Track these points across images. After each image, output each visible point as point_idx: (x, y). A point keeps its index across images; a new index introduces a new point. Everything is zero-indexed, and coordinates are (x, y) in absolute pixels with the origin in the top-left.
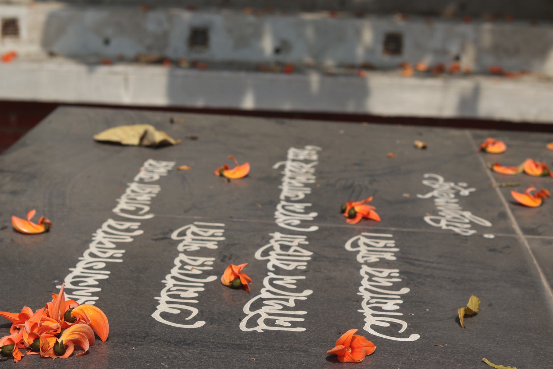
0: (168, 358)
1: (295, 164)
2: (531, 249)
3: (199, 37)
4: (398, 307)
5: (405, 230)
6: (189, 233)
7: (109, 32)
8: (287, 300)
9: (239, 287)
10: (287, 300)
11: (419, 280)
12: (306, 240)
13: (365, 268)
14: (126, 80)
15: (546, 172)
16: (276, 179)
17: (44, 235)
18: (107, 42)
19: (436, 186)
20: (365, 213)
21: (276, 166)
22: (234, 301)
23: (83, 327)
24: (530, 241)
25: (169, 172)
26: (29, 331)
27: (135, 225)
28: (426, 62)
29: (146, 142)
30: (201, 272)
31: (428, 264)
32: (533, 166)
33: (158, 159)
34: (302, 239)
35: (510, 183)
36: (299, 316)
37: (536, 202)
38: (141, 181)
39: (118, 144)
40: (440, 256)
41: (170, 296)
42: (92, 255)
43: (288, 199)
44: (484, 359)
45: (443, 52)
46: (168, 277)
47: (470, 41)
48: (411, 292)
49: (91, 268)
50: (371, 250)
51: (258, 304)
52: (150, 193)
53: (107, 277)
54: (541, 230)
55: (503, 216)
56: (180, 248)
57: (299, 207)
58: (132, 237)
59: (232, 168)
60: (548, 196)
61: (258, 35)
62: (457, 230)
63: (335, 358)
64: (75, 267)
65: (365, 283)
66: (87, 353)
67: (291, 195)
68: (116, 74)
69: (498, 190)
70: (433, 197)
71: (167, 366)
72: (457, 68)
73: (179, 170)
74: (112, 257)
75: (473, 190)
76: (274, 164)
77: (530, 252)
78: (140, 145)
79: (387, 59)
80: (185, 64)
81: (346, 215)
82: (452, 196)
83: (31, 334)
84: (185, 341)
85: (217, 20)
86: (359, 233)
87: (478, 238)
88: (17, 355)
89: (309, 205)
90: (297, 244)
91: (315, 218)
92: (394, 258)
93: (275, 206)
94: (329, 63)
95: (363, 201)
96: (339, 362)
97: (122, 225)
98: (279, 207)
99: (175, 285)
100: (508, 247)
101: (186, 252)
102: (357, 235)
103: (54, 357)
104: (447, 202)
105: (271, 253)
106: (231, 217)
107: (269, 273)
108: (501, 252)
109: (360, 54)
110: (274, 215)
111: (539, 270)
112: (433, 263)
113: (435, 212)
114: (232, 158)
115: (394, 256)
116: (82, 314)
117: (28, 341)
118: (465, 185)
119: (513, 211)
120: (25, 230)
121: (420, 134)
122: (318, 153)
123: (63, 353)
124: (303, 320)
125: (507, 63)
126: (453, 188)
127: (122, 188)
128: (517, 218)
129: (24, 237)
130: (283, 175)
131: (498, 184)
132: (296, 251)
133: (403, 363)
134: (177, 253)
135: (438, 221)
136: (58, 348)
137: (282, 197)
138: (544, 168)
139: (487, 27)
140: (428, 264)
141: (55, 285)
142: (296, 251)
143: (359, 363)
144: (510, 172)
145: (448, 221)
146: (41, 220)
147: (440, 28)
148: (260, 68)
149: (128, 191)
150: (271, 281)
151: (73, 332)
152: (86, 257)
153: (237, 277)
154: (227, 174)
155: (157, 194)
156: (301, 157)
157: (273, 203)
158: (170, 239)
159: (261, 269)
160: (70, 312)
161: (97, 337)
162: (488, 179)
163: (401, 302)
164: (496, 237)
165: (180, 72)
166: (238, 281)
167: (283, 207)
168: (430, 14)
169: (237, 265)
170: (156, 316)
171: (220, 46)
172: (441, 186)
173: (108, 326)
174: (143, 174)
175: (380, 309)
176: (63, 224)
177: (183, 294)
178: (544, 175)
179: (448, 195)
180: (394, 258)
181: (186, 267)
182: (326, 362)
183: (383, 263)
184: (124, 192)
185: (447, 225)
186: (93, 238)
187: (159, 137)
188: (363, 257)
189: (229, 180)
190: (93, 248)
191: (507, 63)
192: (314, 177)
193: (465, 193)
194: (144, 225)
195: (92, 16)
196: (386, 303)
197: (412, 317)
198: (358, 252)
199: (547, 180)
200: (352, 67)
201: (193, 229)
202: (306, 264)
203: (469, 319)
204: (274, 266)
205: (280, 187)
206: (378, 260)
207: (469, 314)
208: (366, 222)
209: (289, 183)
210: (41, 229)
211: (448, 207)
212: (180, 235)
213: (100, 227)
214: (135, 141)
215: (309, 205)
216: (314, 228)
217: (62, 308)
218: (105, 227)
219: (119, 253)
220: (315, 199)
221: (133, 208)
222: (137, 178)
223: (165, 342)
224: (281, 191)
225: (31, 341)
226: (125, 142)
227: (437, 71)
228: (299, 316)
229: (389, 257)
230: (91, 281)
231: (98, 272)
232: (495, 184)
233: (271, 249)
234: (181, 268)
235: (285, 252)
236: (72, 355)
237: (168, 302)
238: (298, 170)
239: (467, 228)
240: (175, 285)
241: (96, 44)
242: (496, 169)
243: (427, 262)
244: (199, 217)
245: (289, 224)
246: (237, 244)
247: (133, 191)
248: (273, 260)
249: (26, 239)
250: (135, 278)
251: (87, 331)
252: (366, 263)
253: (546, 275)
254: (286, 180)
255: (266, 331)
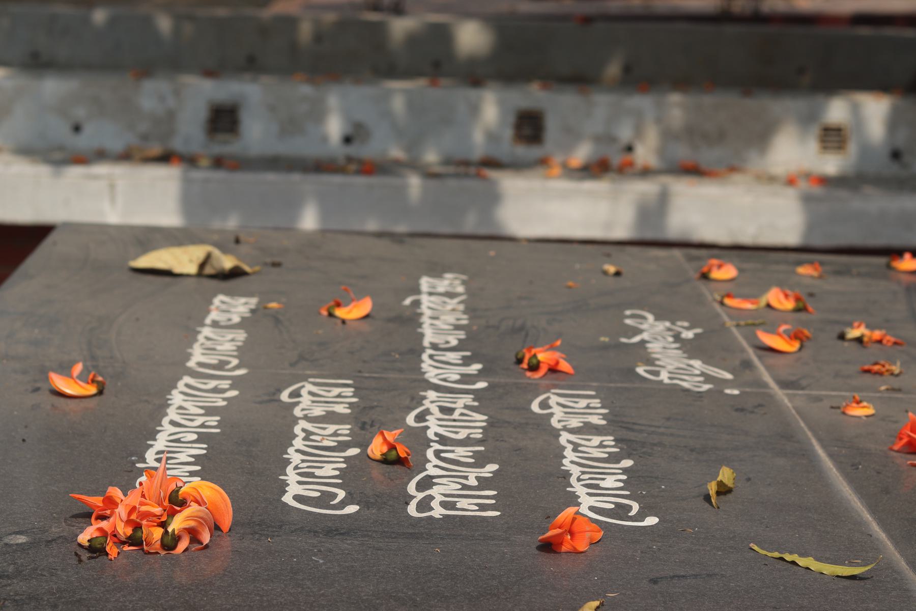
0: (320, 551)
1: (433, 298)
2: (794, 408)
3: (223, 119)
4: (621, 484)
5: (612, 385)
6: (304, 392)
7: (80, 113)
8: (466, 478)
9: (393, 461)
10: (466, 478)
11: (644, 450)
12: (474, 400)
13: (564, 437)
14: (112, 187)
15: (801, 305)
16: (412, 319)
17: (97, 398)
18: (77, 129)
19: (644, 326)
20: (552, 363)
21: (408, 301)
22: (392, 480)
23: (199, 511)
24: (791, 398)
25: (253, 311)
26: (124, 516)
27: (225, 384)
28: (582, 154)
29: (208, 270)
30: (336, 444)
31: (653, 429)
32: (782, 297)
33: (231, 293)
34: (468, 400)
35: (750, 321)
36: (488, 497)
37: (792, 345)
38: (215, 324)
39: (167, 273)
40: (668, 419)
41: (300, 474)
42: (173, 423)
43: (434, 346)
44: (752, 545)
45: (607, 139)
46: (291, 450)
47: (650, 123)
48: (635, 465)
49: (178, 441)
50: (570, 413)
51: (427, 483)
52: (233, 340)
53: (205, 452)
54: (804, 383)
55: (747, 365)
56: (297, 412)
57: (453, 357)
58: (224, 399)
59: (346, 305)
60: (808, 338)
61: (318, 114)
62: (685, 385)
63: (549, 547)
64: (155, 440)
65: (569, 454)
66: (207, 546)
67: (438, 340)
68: (96, 177)
69: (734, 330)
70: (643, 342)
71: (321, 561)
72: (631, 164)
73: (266, 308)
74: (203, 426)
75: (699, 331)
76: (404, 299)
77: (794, 412)
78: (200, 274)
79: (523, 151)
80: (204, 162)
81: (525, 366)
82: (671, 339)
83: (129, 522)
84: (337, 530)
85: (251, 92)
86: (547, 390)
87: (717, 393)
88: (112, 550)
89: (468, 354)
90: (462, 406)
91: (480, 371)
92: (604, 422)
93: (420, 356)
94: (431, 157)
95: (547, 347)
96: (555, 552)
97: (205, 384)
98: (425, 357)
99: (303, 461)
100: (760, 405)
101: (306, 418)
102: (545, 393)
103: (163, 553)
104: (664, 348)
105: (428, 417)
106: (360, 372)
107: (432, 444)
108: (752, 412)
109: (478, 143)
110: (421, 368)
111: (809, 434)
112: (659, 427)
113: (649, 361)
114: (346, 290)
115: (603, 419)
116: (195, 494)
117: (124, 531)
118: (686, 324)
119: (760, 358)
120: (69, 391)
121: (608, 255)
122: (464, 283)
123: (174, 547)
124: (493, 502)
125: (707, 156)
126: (669, 329)
127: (191, 336)
128: (768, 368)
129: (69, 401)
130: (421, 314)
131: (734, 323)
132: (462, 414)
133: (642, 552)
134: (295, 420)
135: (657, 373)
136: (168, 540)
137: (426, 343)
138: (798, 299)
139: (675, 98)
140: (653, 429)
141: (134, 463)
142: (462, 414)
143: (582, 552)
144: (748, 306)
145: (670, 373)
146: (91, 377)
147: (602, 102)
148: (321, 166)
149: (201, 338)
150: (437, 454)
151: (188, 518)
152: (167, 428)
153: (392, 447)
154: (340, 313)
155: (244, 342)
156: (441, 289)
157: (417, 351)
158: (280, 401)
159: (419, 438)
160: (178, 491)
161: (217, 528)
162: (718, 315)
163: (624, 477)
164: (742, 393)
165: (197, 175)
166: (394, 452)
167: (431, 357)
168: (582, 80)
169: (391, 431)
170: (288, 499)
171: (256, 133)
172: (652, 326)
173: (231, 510)
174: (214, 315)
175: (597, 487)
176: (119, 384)
177: (318, 472)
178: (797, 310)
179: (664, 338)
180: (604, 422)
181: (312, 437)
182: (537, 552)
183: (588, 429)
184: (196, 340)
185: (670, 378)
186: (169, 402)
187: (228, 263)
188: (559, 421)
189: (344, 322)
190: (172, 414)
191: (707, 156)
192: (465, 317)
193: (689, 335)
194: (236, 383)
195: (52, 87)
196: (604, 479)
197: (644, 496)
198: (552, 414)
199: (802, 316)
200: (466, 163)
201: (309, 387)
202: (481, 431)
203: (722, 497)
204: (436, 434)
205: (419, 330)
206: (581, 424)
207: (724, 490)
208: (554, 376)
209: (432, 325)
210: (93, 390)
211: (668, 355)
212: (291, 395)
213: (175, 387)
214: (192, 269)
215: (468, 354)
216: (482, 385)
217: (164, 487)
218: (181, 385)
219: (213, 420)
220: (473, 345)
221: (214, 362)
222: (208, 321)
223: (309, 531)
224: (422, 335)
225: (129, 531)
226: (178, 269)
227: (597, 168)
228: (488, 497)
229: (596, 420)
230: (183, 458)
231: (189, 445)
232: (729, 323)
233: (427, 412)
234: (305, 439)
235: (448, 415)
236: (186, 550)
237: (299, 483)
238: (440, 308)
239: (699, 382)
240: (303, 461)
241: (60, 131)
242: (727, 301)
243: (650, 426)
244: (315, 372)
245: (445, 380)
246: (377, 406)
247: (208, 339)
248: (434, 427)
249: (72, 404)
250: (245, 450)
251: (205, 517)
252: (565, 429)
253: (820, 440)
254: (426, 320)
255: (446, 517)
